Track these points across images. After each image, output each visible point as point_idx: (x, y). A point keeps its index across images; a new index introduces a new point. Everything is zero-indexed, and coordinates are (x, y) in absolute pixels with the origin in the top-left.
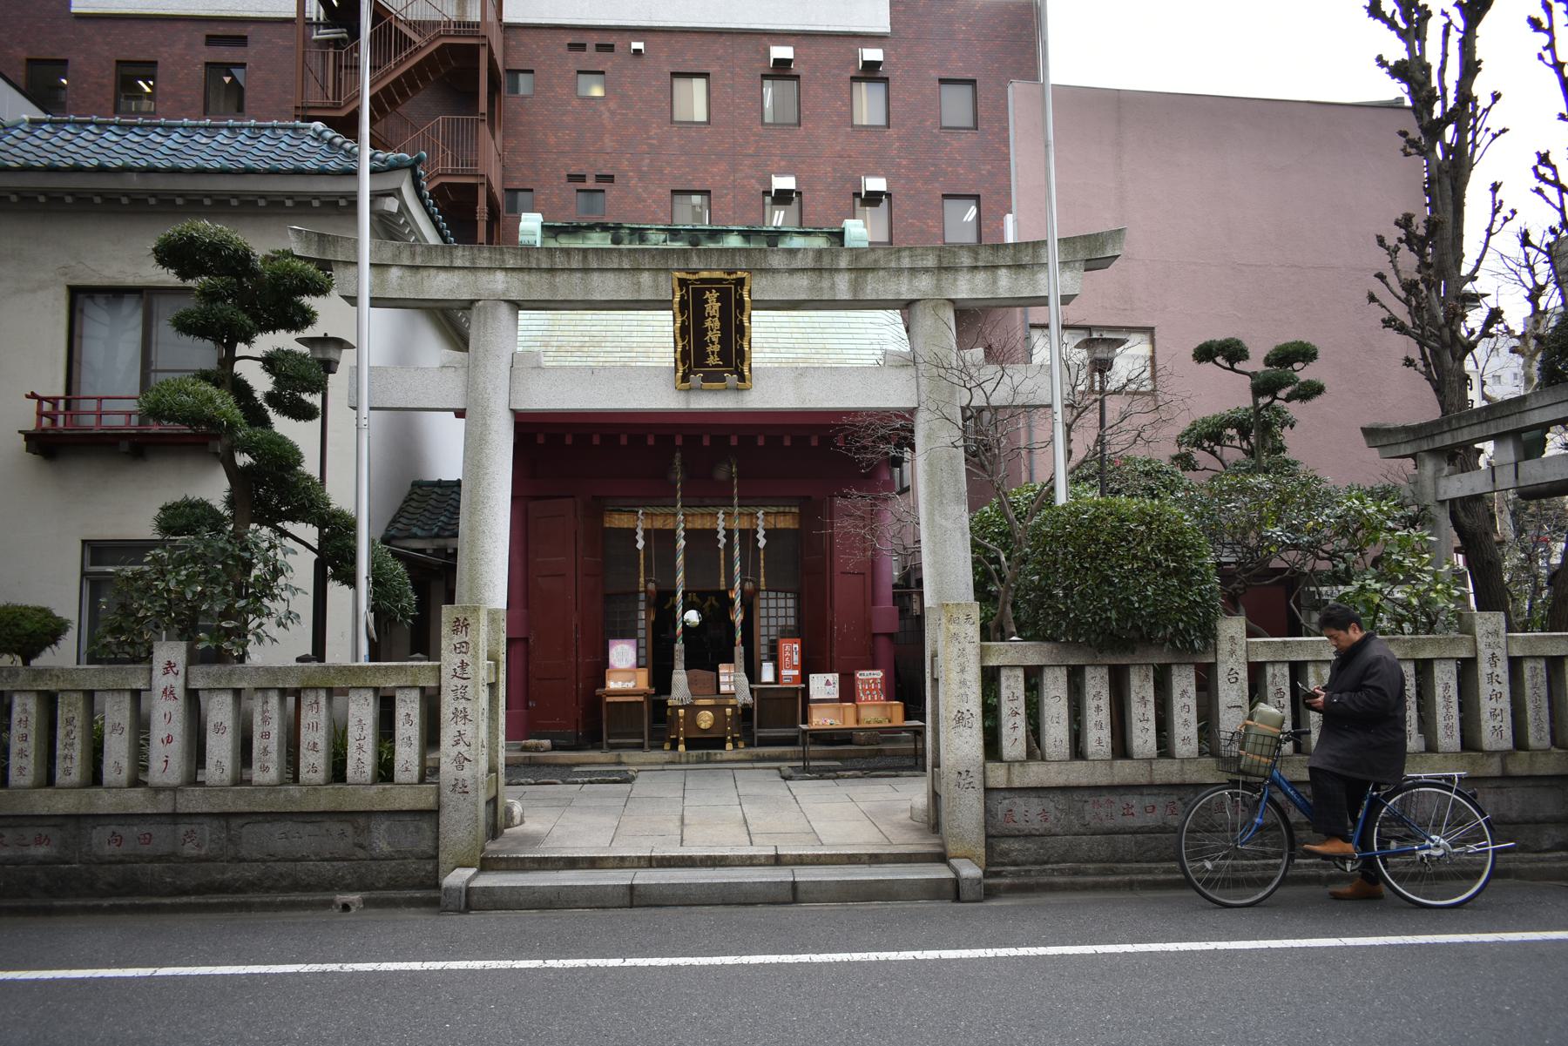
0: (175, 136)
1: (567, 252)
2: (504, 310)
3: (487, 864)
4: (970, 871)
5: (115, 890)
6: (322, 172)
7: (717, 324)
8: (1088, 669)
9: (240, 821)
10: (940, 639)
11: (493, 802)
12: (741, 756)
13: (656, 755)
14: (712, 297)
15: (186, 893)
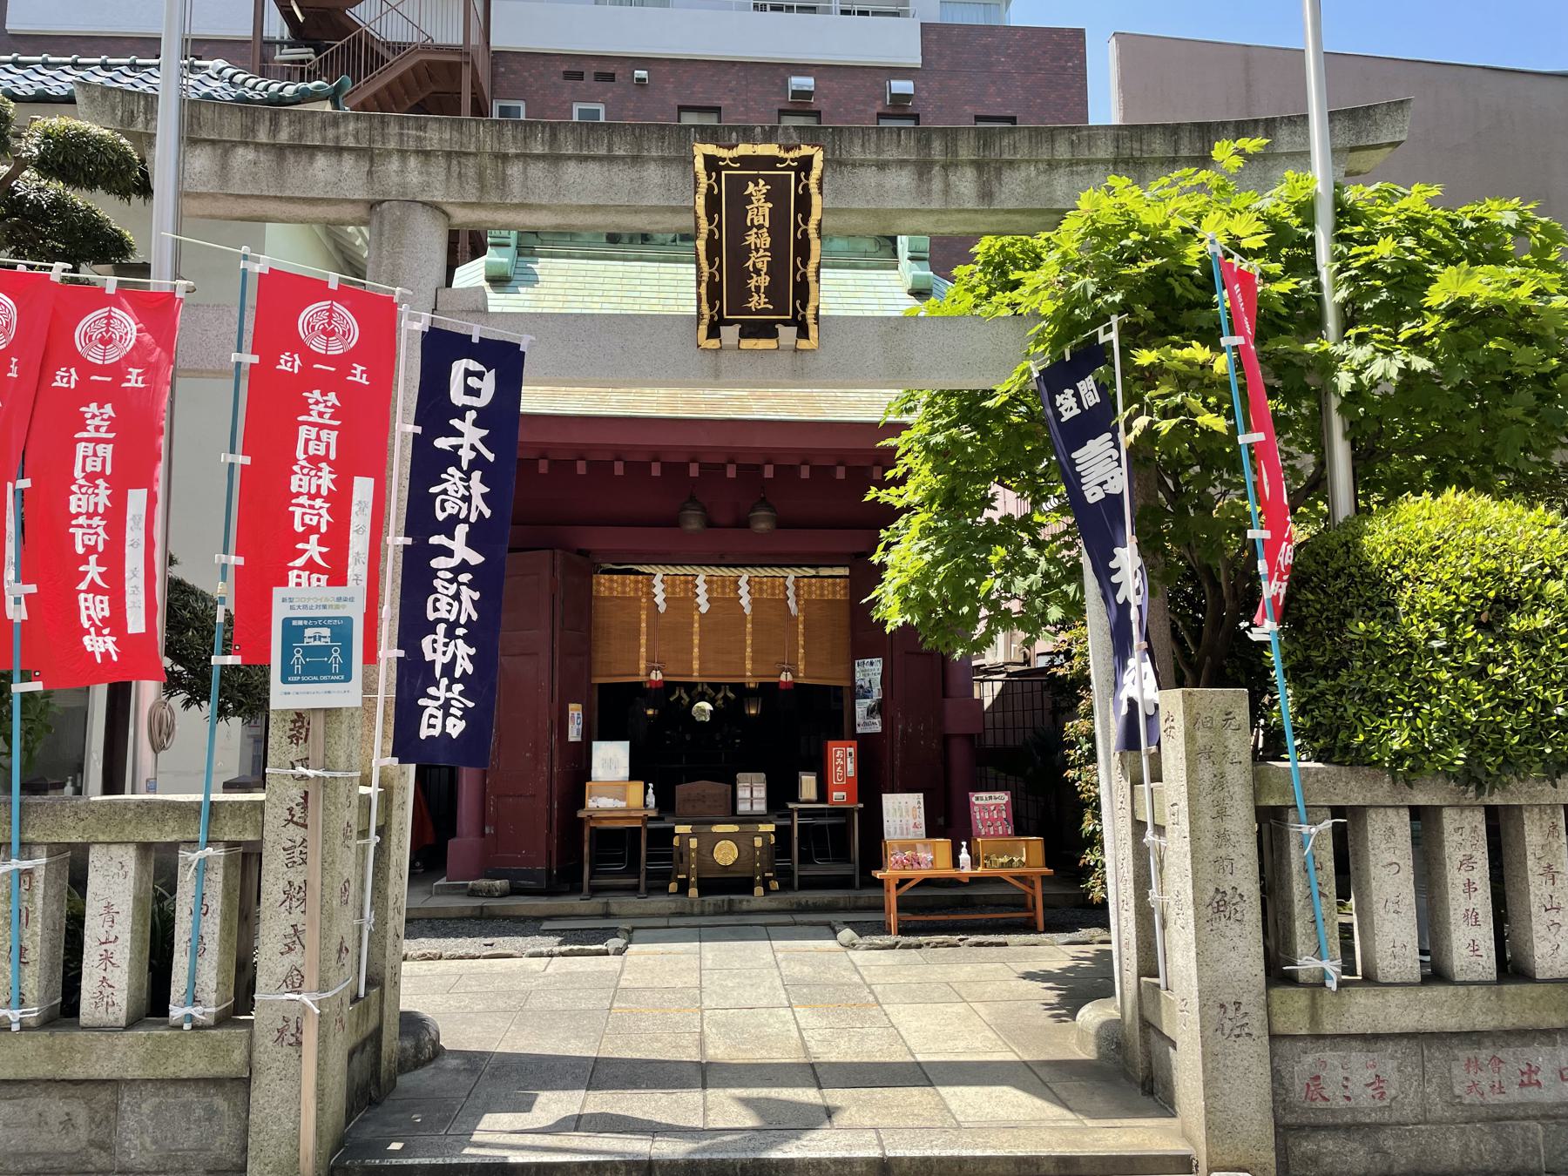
7: (766, 241)
8: (1447, 813)
12: (774, 905)
13: (659, 903)
14: (757, 191)
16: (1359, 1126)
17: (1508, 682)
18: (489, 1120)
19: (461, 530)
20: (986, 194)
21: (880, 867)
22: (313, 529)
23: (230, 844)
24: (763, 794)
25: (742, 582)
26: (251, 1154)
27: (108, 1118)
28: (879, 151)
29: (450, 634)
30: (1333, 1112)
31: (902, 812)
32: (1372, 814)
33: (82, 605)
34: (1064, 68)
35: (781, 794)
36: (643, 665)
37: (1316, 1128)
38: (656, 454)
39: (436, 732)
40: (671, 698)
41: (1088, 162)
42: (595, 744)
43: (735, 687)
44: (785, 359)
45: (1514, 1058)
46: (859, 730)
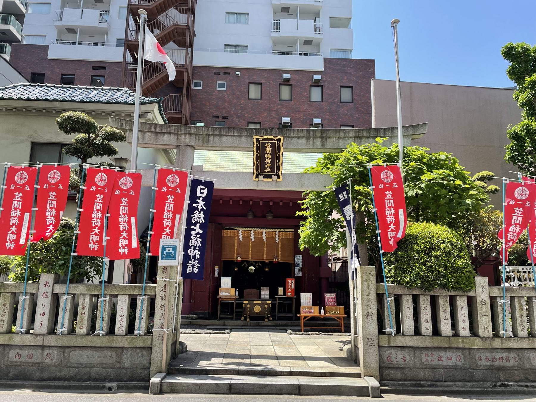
5: (16, 377)
6: (126, 103)
8: (421, 296)
9: (69, 350)
12: (270, 324)
13: (238, 322)
14: (268, 146)
15: (44, 380)
16: (400, 368)
17: (431, 267)
18: (201, 362)
19: (198, 225)
20: (323, 145)
21: (300, 313)
22: (168, 226)
23: (149, 295)
24: (268, 293)
25: (264, 233)
27: (120, 356)
28: (298, 134)
29: (195, 249)
30: (393, 364)
31: (306, 298)
32: (404, 296)
33: (120, 241)
34: (368, 72)
35: (273, 293)
36: (235, 256)
37: (390, 368)
38: (241, 198)
39: (191, 271)
40: (243, 265)
41: (348, 137)
42: (222, 278)
43: (261, 262)
44: (274, 183)
45: (437, 354)
46: (296, 276)
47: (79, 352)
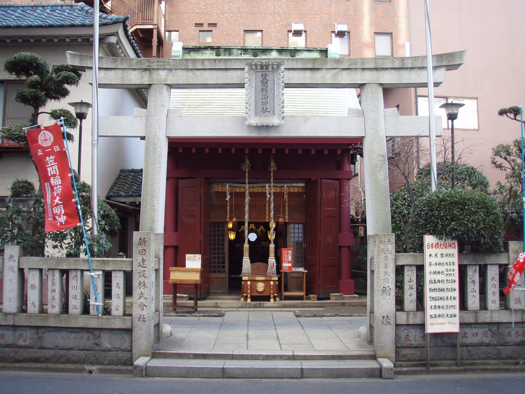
0: (19, 11)
1: (194, 60)
2: (165, 87)
3: (154, 355)
4: (387, 364)
9: (43, 330)
10: (375, 251)
11: (157, 326)
12: (275, 305)
26: (133, 347)
47: (54, 334)
